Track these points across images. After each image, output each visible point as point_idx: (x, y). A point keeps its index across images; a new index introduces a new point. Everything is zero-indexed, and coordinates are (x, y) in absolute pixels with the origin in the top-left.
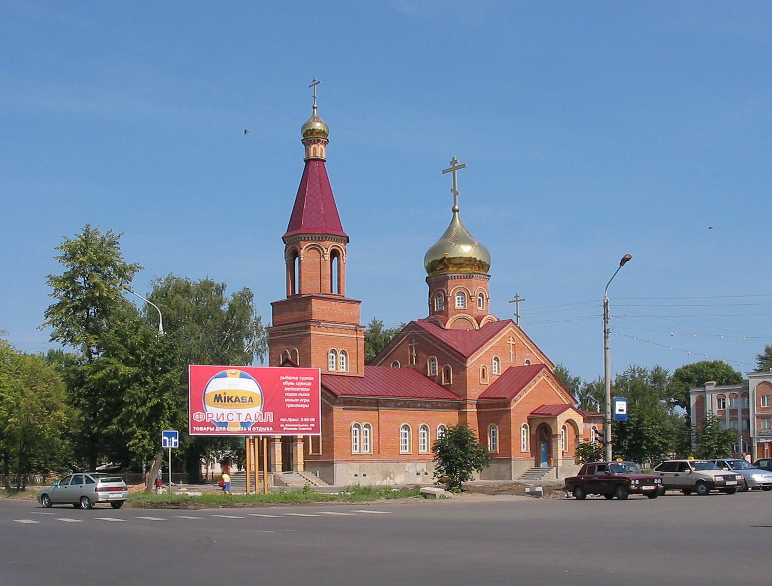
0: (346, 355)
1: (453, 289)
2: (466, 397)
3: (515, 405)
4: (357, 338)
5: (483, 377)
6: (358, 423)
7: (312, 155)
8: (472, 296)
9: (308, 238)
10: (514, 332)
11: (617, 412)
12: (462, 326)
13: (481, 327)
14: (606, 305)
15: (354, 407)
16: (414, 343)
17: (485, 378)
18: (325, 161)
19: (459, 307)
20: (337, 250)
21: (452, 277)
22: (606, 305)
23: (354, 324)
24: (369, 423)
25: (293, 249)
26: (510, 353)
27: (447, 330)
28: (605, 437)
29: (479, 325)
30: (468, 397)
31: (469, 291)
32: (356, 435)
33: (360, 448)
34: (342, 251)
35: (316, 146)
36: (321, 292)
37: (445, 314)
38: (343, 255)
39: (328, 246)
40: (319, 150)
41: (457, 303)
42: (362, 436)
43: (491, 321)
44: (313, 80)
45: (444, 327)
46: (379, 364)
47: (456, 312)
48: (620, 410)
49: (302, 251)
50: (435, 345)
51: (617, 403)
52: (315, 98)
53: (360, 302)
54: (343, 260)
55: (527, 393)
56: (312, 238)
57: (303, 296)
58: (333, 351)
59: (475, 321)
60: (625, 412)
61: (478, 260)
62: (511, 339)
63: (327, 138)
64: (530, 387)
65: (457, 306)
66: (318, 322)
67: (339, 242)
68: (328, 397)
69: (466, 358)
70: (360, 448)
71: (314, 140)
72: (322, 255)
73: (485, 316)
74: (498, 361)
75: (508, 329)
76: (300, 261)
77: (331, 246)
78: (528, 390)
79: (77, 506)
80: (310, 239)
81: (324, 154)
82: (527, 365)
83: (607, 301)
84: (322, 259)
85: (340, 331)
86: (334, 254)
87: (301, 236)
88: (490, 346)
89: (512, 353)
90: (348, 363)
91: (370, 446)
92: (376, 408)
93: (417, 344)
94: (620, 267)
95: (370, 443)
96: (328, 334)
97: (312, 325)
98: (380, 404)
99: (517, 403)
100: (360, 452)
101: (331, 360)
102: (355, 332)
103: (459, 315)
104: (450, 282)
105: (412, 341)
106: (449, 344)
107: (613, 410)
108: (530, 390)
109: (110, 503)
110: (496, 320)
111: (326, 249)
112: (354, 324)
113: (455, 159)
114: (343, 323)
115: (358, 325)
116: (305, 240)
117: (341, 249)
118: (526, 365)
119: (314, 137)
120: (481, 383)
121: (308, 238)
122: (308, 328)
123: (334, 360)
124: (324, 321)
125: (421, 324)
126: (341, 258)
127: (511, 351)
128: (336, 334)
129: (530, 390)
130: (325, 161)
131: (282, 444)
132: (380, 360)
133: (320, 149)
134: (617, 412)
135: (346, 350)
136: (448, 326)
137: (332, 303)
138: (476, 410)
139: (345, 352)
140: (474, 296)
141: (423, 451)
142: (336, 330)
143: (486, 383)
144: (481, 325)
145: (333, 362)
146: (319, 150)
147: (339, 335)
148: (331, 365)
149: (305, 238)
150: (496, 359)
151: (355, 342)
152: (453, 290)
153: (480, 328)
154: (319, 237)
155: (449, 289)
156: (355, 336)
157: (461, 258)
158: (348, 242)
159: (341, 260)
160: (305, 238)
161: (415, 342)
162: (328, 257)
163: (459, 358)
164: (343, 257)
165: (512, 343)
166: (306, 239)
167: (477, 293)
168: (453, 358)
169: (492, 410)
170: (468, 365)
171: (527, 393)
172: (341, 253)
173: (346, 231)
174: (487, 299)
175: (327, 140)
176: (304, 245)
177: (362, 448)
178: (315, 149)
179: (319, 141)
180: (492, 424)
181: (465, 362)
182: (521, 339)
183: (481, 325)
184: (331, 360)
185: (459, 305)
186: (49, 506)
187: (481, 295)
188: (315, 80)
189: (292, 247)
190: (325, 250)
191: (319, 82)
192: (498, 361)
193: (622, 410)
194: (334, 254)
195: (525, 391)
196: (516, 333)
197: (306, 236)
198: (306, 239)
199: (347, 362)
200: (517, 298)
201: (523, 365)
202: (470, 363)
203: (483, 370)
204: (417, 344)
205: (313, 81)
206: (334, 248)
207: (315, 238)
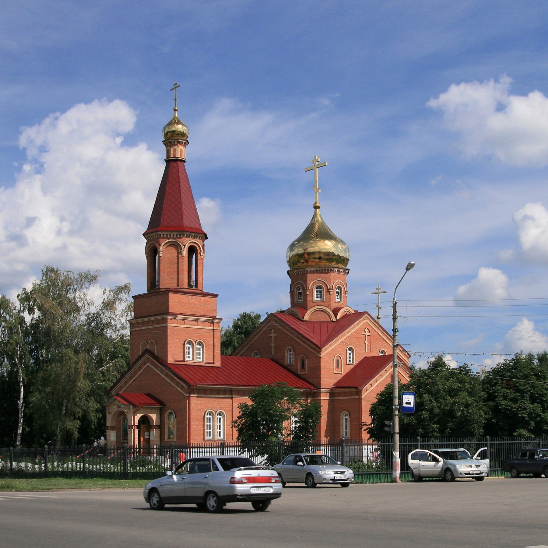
0: (203, 347)
1: (313, 280)
2: (320, 387)
3: (366, 393)
4: (213, 330)
5: (338, 367)
6: (212, 411)
7: (172, 156)
8: (330, 289)
9: (167, 235)
10: (370, 324)
11: (404, 405)
12: (322, 317)
13: (338, 318)
14: (395, 306)
15: (208, 396)
16: (273, 333)
17: (340, 367)
18: (184, 161)
19: (317, 299)
20: (195, 246)
21: (310, 270)
22: (395, 306)
23: (211, 317)
24: (222, 411)
25: (152, 246)
26: (365, 343)
27: (305, 321)
28: (392, 428)
29: (336, 316)
30: (321, 386)
31: (328, 285)
32: (209, 422)
33: (213, 435)
34: (200, 248)
35: (176, 147)
36: (178, 286)
37: (304, 307)
38: (201, 251)
39: (186, 242)
40: (180, 151)
41: (315, 296)
42: (216, 422)
43: (348, 313)
44: (174, 83)
45: (301, 318)
46: (241, 354)
47: (314, 304)
48: (407, 403)
49: (161, 248)
50: (292, 336)
51: (405, 397)
52: (176, 100)
53: (217, 296)
54: (201, 256)
55: (378, 382)
56: (170, 235)
57: (161, 290)
58: (190, 343)
59: (332, 314)
60: (412, 405)
61: (336, 255)
62: (366, 330)
63: (187, 140)
64: (382, 376)
65: (315, 299)
66: (175, 315)
67: (197, 239)
68: (183, 386)
69: (320, 348)
70: (213, 435)
71: (174, 142)
72: (179, 251)
73: (342, 308)
74: (353, 352)
75: (362, 321)
76: (159, 257)
77: (188, 243)
78: (380, 379)
79: (202, 508)
80: (169, 236)
81: (183, 155)
82: (382, 355)
83: (396, 302)
84: (180, 255)
85: (190, 322)
86: (192, 250)
87: (160, 233)
88: (345, 337)
89: (367, 343)
90: (205, 354)
91: (224, 432)
92: (230, 396)
93: (276, 335)
94: (406, 272)
95: (224, 430)
96: (185, 326)
97: (169, 317)
98: (233, 393)
99: (368, 392)
100: (213, 438)
101: (188, 351)
102: (212, 324)
103: (317, 307)
104: (309, 276)
105: (272, 332)
106: (305, 335)
107: (400, 403)
108: (382, 379)
109: (250, 503)
110: (353, 312)
111: (183, 245)
112: (211, 317)
113: (317, 158)
114: (201, 316)
115: (214, 318)
116: (164, 238)
117: (199, 246)
118: (381, 354)
119: (174, 138)
120: (335, 372)
121: (167, 235)
122: (165, 321)
123: (191, 351)
124: (181, 314)
125: (281, 317)
126: (199, 253)
127: (366, 342)
128: (193, 327)
129: (382, 379)
130: (184, 161)
131: (138, 430)
132: (243, 350)
133: (179, 150)
134: (404, 405)
135: (202, 341)
136: (306, 318)
137: (189, 298)
138: (328, 398)
139: (202, 343)
140: (332, 289)
141: (219, 438)
142: (193, 322)
143: (341, 373)
144: (338, 317)
145: (189, 353)
146: (180, 151)
147: (196, 327)
148: (188, 355)
149: (164, 235)
150: (351, 349)
151: (212, 333)
152: (312, 283)
153: (337, 320)
154: (177, 235)
155: (308, 282)
156: (212, 328)
157: (320, 252)
158: (207, 238)
159: (199, 255)
160: (164, 235)
161: (274, 333)
162: (185, 253)
163: (315, 349)
164: (200, 254)
165: (367, 333)
166: (165, 236)
167: (335, 286)
168: (308, 348)
169: (345, 398)
170: (322, 355)
171: (378, 382)
172: (198, 249)
173: (205, 229)
174: (345, 292)
175: (187, 141)
176: (163, 242)
177: (216, 434)
178: (175, 150)
179: (179, 142)
180: (345, 411)
181: (319, 352)
182: (376, 330)
183: (338, 317)
184: (188, 351)
185: (317, 297)
186: (160, 506)
187: (339, 288)
188: (176, 84)
189: (152, 243)
190: (183, 247)
191: (179, 86)
192: (353, 352)
193: (410, 403)
194: (192, 250)
195: (376, 381)
196: (371, 325)
197: (165, 233)
198: (165, 236)
199: (203, 353)
200: (379, 291)
201: (378, 355)
202: (325, 352)
203: (338, 361)
204: (276, 335)
205: (174, 85)
206: (192, 244)
207: (173, 235)
